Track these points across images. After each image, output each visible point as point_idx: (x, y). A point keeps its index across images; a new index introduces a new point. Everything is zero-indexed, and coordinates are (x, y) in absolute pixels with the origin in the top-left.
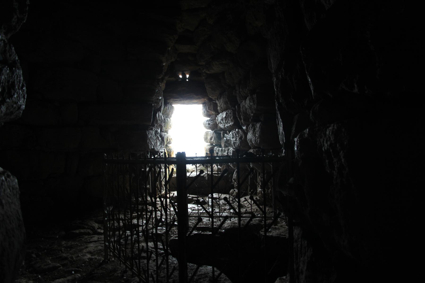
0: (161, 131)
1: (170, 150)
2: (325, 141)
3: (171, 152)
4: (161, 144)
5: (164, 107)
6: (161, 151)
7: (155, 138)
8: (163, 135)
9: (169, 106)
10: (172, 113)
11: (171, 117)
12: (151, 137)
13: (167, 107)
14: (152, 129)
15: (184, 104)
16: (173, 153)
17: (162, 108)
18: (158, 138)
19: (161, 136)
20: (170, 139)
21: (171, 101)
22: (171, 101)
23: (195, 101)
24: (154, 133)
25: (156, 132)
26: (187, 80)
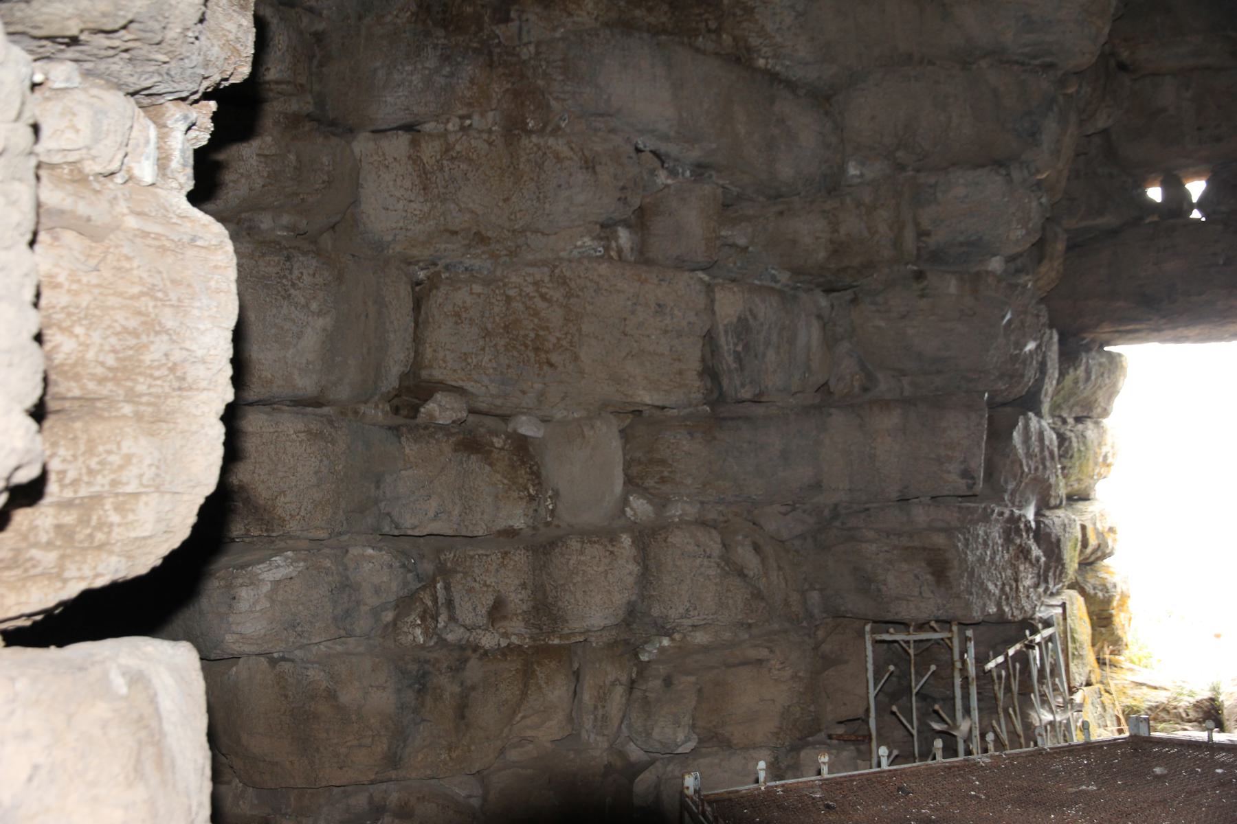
0: (1044, 505)
1: (1105, 589)
2: (153, 400)
3: (1108, 601)
4: (1042, 578)
5: (1062, 374)
6: (1042, 613)
7: (1003, 557)
8: (1057, 531)
9: (1091, 360)
10: (1112, 393)
11: (1105, 413)
12: (981, 560)
13: (1081, 372)
14: (986, 518)
15: (1177, 340)
16: (1122, 604)
17: (1050, 386)
18: (1024, 552)
19: (1040, 534)
20: (1100, 534)
21: (1105, 337)
22: (1104, 331)
23: (1196, 330)
24: (996, 533)
25: (1013, 526)
26: (1196, 214)
